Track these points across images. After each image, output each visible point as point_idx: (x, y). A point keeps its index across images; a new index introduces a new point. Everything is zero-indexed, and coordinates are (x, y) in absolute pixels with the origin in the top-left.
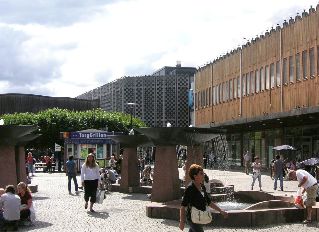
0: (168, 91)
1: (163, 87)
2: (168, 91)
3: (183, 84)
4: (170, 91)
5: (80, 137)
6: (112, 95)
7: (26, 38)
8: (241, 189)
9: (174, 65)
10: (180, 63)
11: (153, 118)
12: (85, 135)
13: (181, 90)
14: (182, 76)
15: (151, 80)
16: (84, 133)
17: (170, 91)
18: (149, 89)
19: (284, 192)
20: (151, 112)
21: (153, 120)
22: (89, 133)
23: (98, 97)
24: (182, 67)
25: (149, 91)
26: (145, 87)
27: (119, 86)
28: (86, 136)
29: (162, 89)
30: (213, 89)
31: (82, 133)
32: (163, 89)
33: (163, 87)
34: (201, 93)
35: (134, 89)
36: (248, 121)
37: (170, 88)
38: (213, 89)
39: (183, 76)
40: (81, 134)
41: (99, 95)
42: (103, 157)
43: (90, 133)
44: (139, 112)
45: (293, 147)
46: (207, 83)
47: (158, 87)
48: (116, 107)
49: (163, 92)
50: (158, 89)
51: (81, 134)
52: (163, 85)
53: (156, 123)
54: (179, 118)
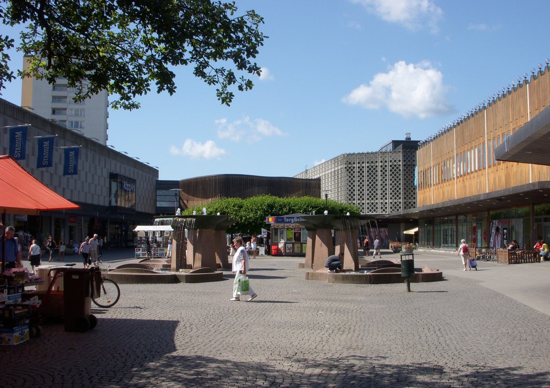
0: (393, 168)
1: (387, 164)
2: (393, 168)
3: (409, 161)
4: (395, 168)
5: (285, 221)
6: (333, 173)
7: (179, 64)
8: (521, 266)
9: (403, 138)
10: (410, 135)
11: (377, 199)
12: (290, 219)
13: (407, 168)
14: (408, 151)
15: (407, 153)
16: (289, 218)
17: (395, 168)
18: (372, 167)
19: (108, 185)
20: (375, 192)
21: (376, 201)
22: (293, 218)
23: (318, 176)
24: (412, 140)
25: (372, 169)
26: (367, 165)
27: (339, 164)
28: (291, 220)
29: (363, 167)
30: (433, 169)
31: (287, 218)
32: (387, 167)
33: (387, 164)
34: (423, 171)
35: (355, 167)
36: (446, 195)
37: (395, 166)
38: (433, 169)
39: (409, 152)
40: (285, 218)
41: (320, 174)
42: (42, 172)
43: (294, 217)
44: (361, 192)
45: (181, 189)
46: (428, 162)
47: (382, 164)
48: (336, 187)
49: (387, 170)
50: (359, 167)
51: (285, 218)
52: (387, 161)
53: (380, 204)
54: (405, 198)
